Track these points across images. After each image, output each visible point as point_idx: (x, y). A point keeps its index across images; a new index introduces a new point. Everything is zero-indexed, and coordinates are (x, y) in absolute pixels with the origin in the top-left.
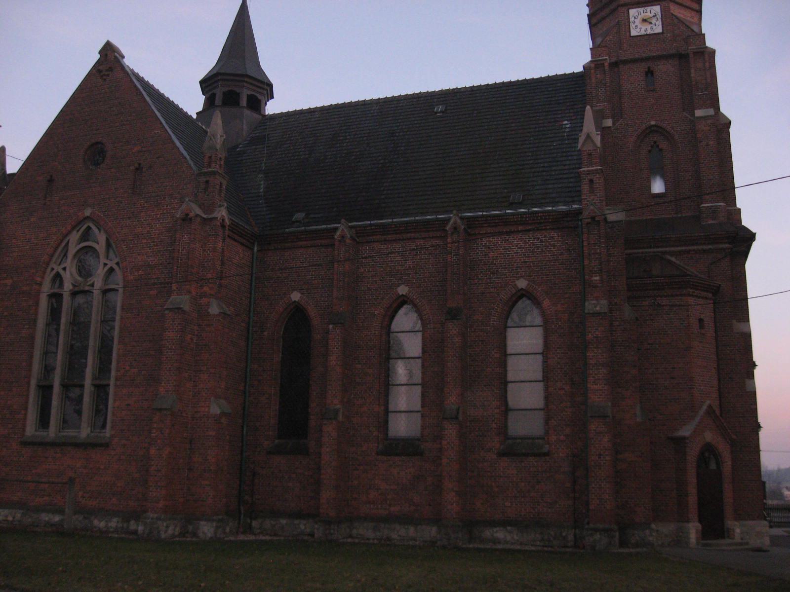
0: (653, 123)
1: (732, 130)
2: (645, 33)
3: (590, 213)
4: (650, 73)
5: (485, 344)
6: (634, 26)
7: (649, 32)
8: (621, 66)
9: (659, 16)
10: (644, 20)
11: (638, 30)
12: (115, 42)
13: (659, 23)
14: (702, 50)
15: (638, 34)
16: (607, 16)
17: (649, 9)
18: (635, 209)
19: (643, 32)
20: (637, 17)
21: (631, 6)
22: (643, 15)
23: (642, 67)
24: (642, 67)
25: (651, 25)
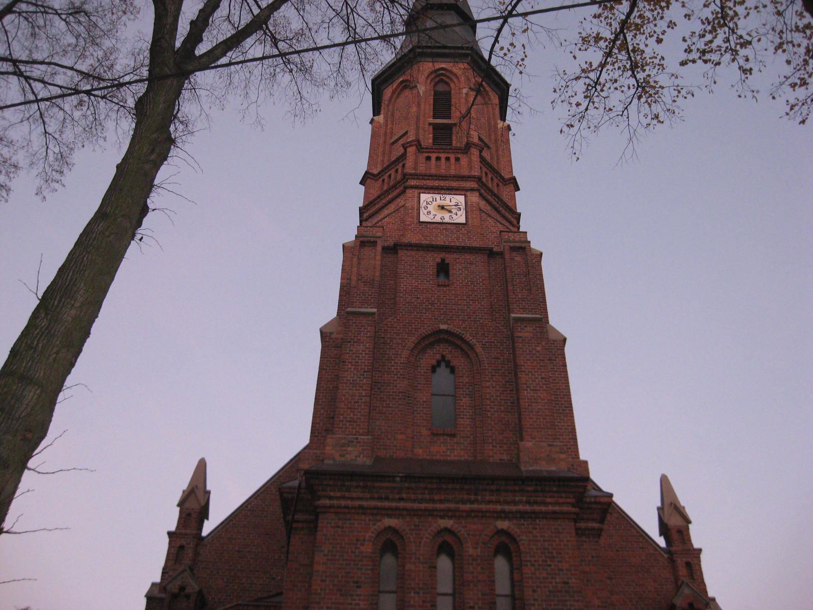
0: (443, 327)
1: (568, 349)
2: (440, 221)
3: (253, 507)
4: (443, 269)
5: (509, 402)
6: (425, 212)
7: (447, 220)
8: (401, 253)
9: (463, 207)
10: (442, 208)
11: (431, 216)
12: (666, 474)
13: (462, 213)
14: (523, 245)
15: (432, 221)
16: (493, 479)
17: (448, 197)
18: (288, 553)
19: (438, 219)
20: (430, 203)
21: (423, 191)
22: (439, 202)
23: (433, 259)
24: (433, 259)
25: (450, 214)
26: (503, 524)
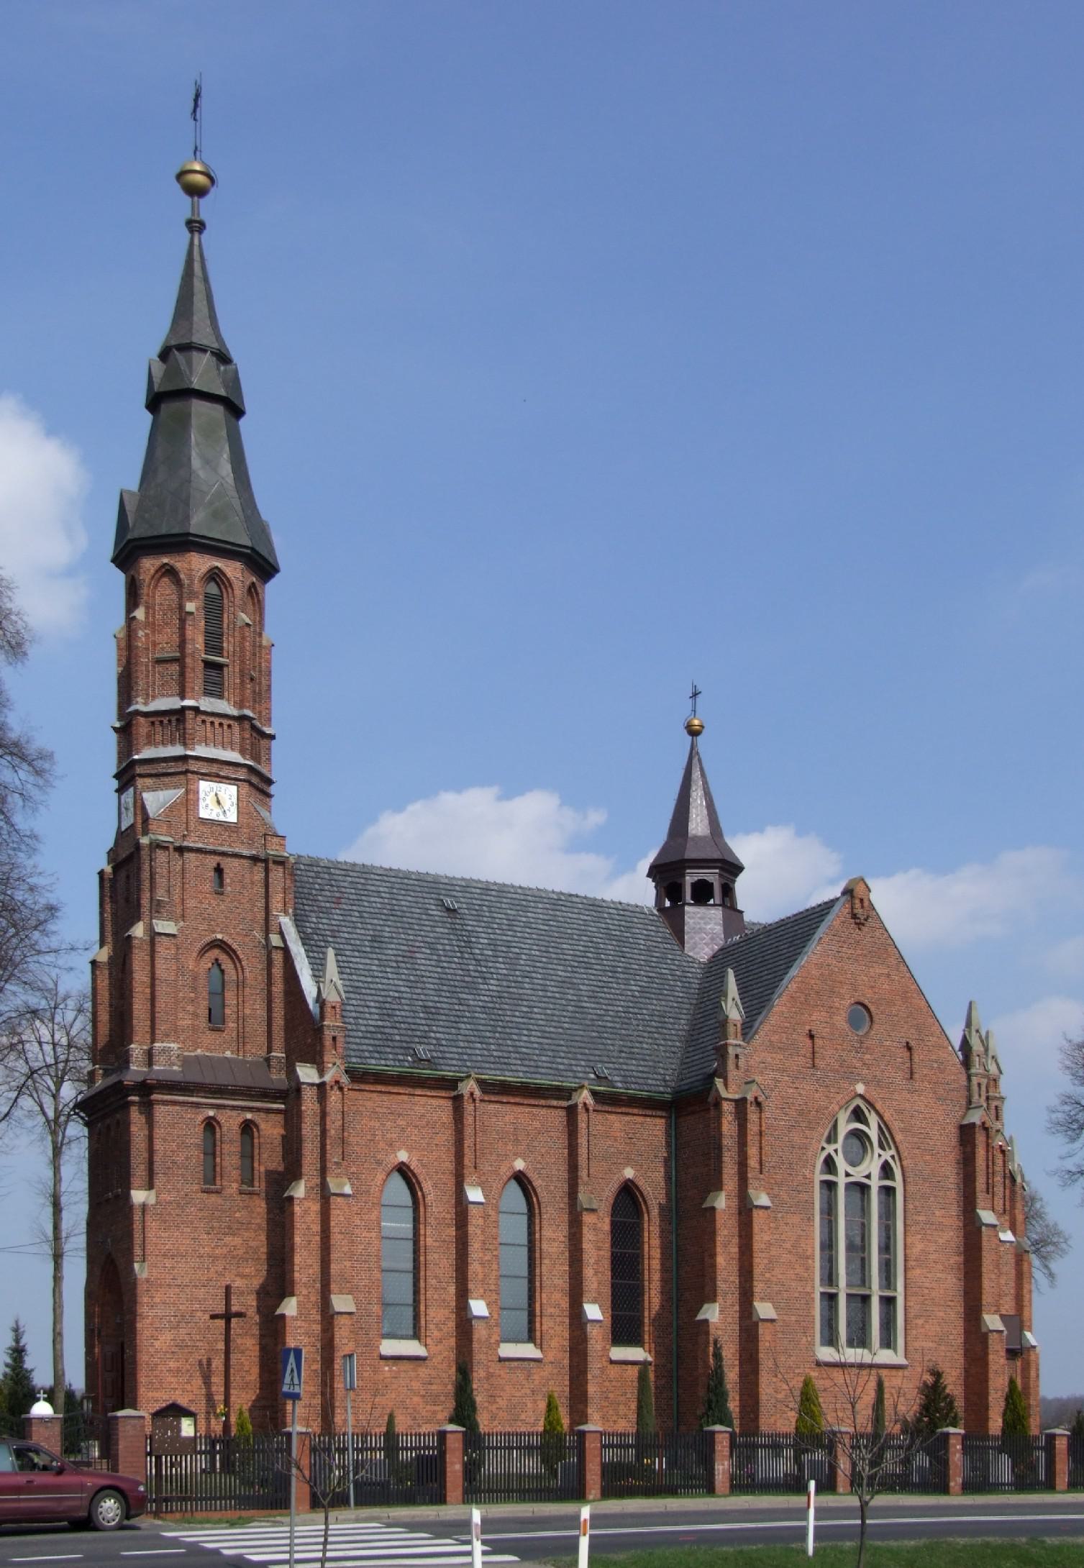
0: (219, 936)
26: (249, 1116)
